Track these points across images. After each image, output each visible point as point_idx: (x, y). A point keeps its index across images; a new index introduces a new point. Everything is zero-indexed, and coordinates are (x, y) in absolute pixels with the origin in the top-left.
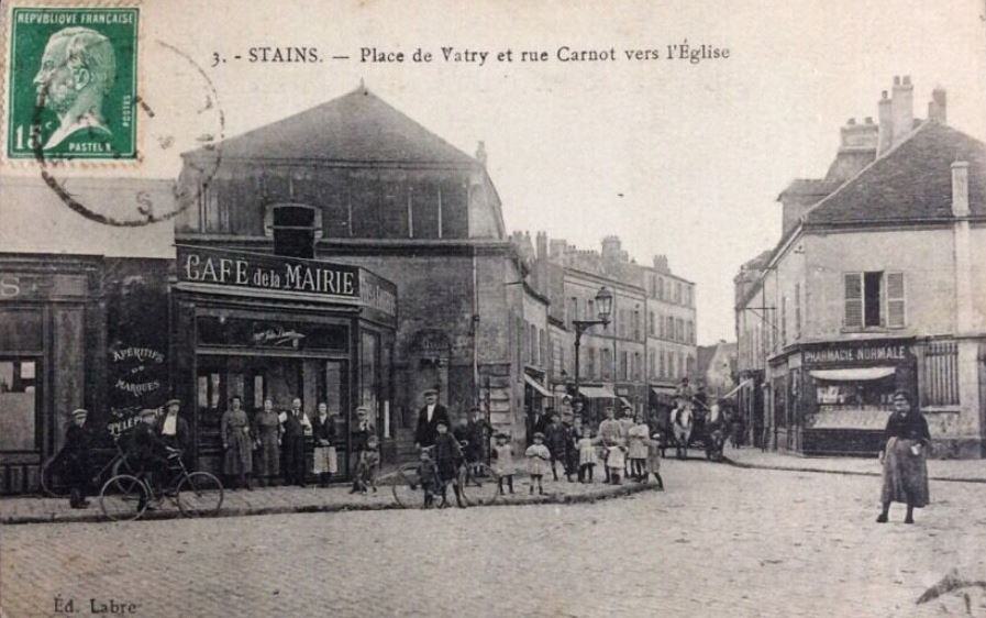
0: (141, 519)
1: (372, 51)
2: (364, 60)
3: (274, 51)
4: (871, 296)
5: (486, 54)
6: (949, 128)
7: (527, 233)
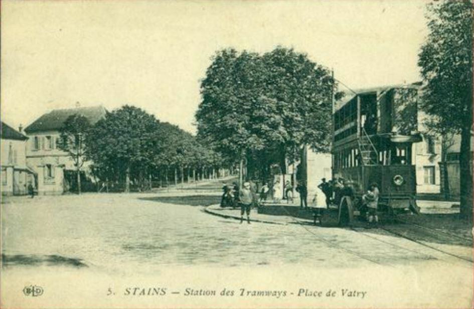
0: (104, 190)
1: (305, 291)
2: (299, 295)
3: (141, 290)
4: (275, 210)
5: (366, 292)
6: (113, 111)
7: (332, 69)
